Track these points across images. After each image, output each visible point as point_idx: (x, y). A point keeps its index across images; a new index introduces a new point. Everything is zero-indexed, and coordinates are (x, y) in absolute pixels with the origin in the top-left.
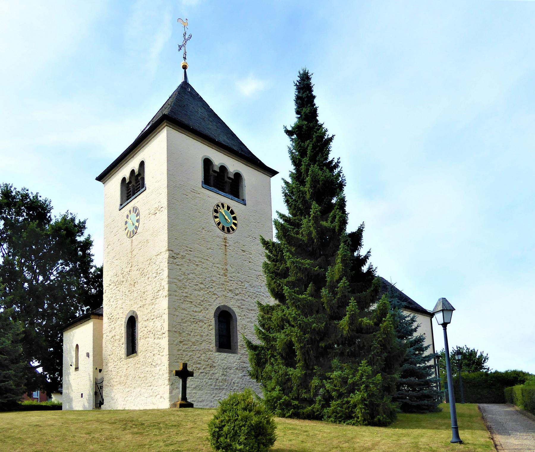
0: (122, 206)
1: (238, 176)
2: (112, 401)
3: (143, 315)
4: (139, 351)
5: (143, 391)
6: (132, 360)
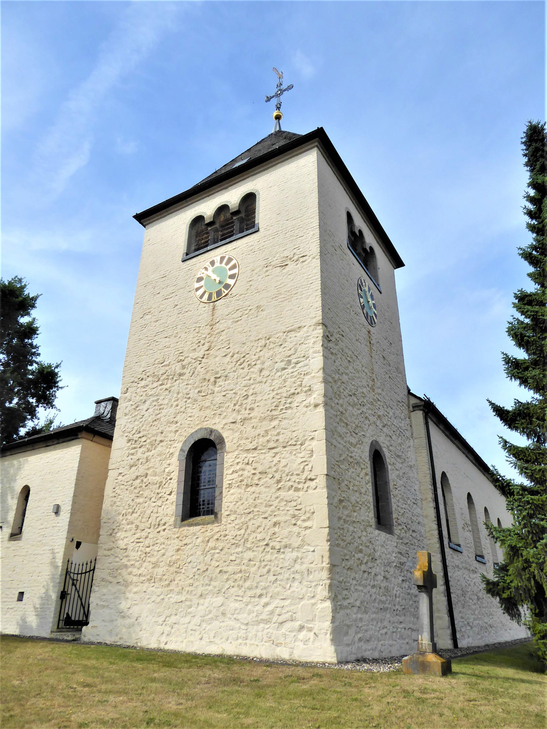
0: (189, 257)
2: (120, 621)
3: (240, 439)
4: (224, 512)
5: (234, 605)
6: (199, 531)
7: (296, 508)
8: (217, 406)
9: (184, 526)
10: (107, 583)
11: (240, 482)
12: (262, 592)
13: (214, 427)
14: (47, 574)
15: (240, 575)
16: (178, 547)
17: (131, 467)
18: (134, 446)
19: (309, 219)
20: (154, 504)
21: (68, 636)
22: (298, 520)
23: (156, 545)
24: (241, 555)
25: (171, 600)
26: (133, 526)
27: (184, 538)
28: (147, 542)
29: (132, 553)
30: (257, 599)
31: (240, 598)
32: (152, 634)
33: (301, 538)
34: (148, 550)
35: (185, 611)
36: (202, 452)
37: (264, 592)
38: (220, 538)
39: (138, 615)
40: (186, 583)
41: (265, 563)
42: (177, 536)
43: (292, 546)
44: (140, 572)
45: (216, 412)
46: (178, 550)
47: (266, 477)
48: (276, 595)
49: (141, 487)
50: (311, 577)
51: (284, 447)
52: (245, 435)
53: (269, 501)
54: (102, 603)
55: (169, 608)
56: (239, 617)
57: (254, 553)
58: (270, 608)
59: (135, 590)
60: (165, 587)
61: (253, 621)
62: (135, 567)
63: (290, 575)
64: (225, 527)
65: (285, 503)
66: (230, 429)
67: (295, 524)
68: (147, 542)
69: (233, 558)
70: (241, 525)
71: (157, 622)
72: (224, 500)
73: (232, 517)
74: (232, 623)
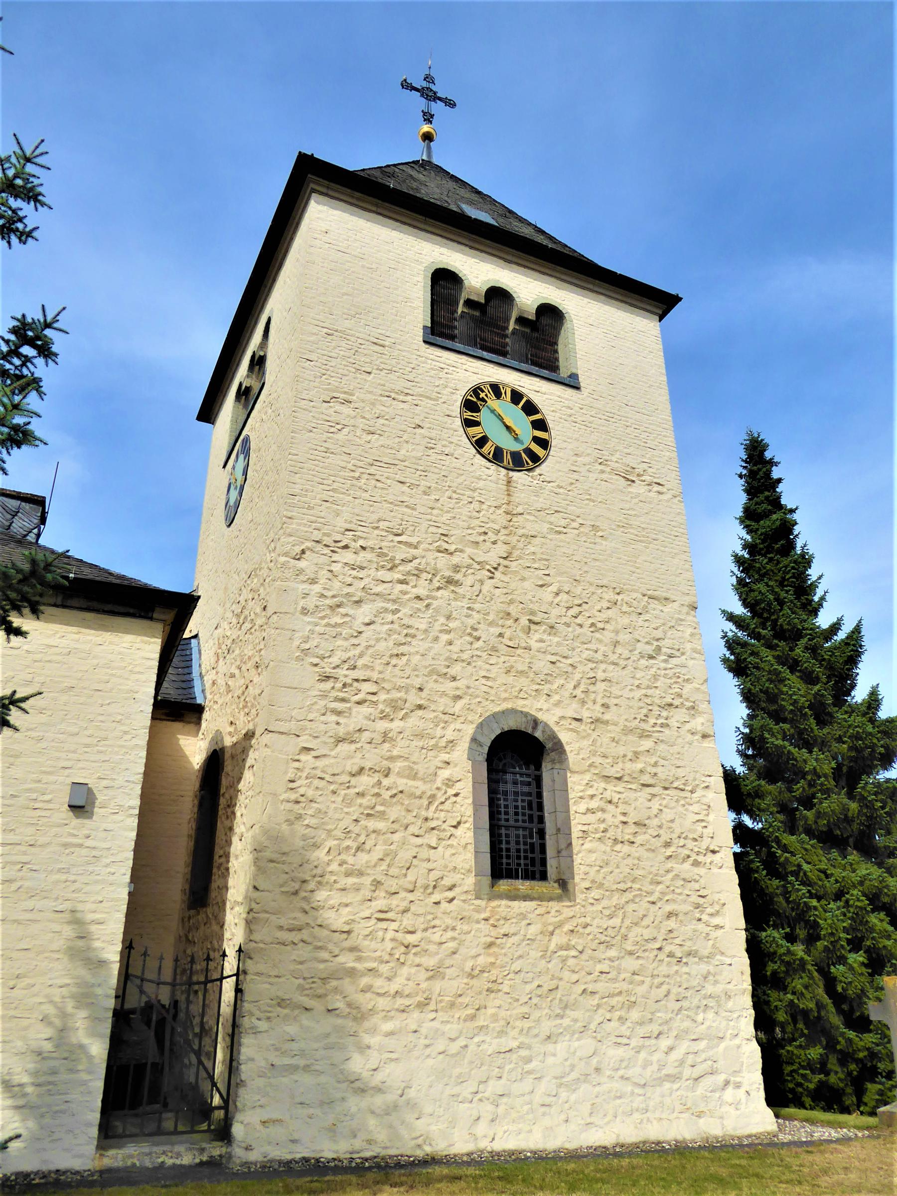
1: (550, 315)
2: (354, 1103)
3: (594, 753)
7: (700, 893)
8: (542, 677)
9: (500, 897)
10: (296, 1012)
11: (603, 832)
12: (661, 1028)
13: (540, 716)
14: (61, 982)
15: (620, 999)
16: (489, 939)
17: (340, 740)
18: (341, 695)
19: (658, 426)
20: (419, 841)
21: (178, 1155)
22: (702, 912)
23: (430, 931)
24: (617, 963)
25: (484, 1046)
26: (367, 881)
27: (502, 922)
28: (407, 921)
29: (366, 943)
30: (653, 1041)
31: (625, 1041)
32: (453, 1124)
33: (711, 942)
34: (410, 939)
35: (520, 1070)
36: (517, 758)
37: (665, 1028)
38: (576, 929)
39: (404, 1084)
40: (515, 1012)
41: (661, 980)
42: (483, 916)
43: (699, 954)
44: (394, 987)
45: (540, 687)
46: (490, 945)
47: (645, 833)
48: (684, 1034)
49: (378, 795)
50: (730, 1004)
51: (666, 789)
52: (602, 750)
53: (656, 875)
54: (287, 1061)
55: (482, 1064)
56: (630, 1073)
57: (640, 962)
58: (675, 1055)
59: (388, 1026)
60: (465, 1020)
61: (655, 1079)
62: (380, 976)
63: (700, 1000)
64: (583, 910)
65: (682, 883)
66: (571, 730)
67: (700, 920)
68: (407, 921)
69: (604, 967)
70: (613, 909)
71: (458, 1096)
72: (577, 859)
73: (595, 894)
74: (616, 1085)
